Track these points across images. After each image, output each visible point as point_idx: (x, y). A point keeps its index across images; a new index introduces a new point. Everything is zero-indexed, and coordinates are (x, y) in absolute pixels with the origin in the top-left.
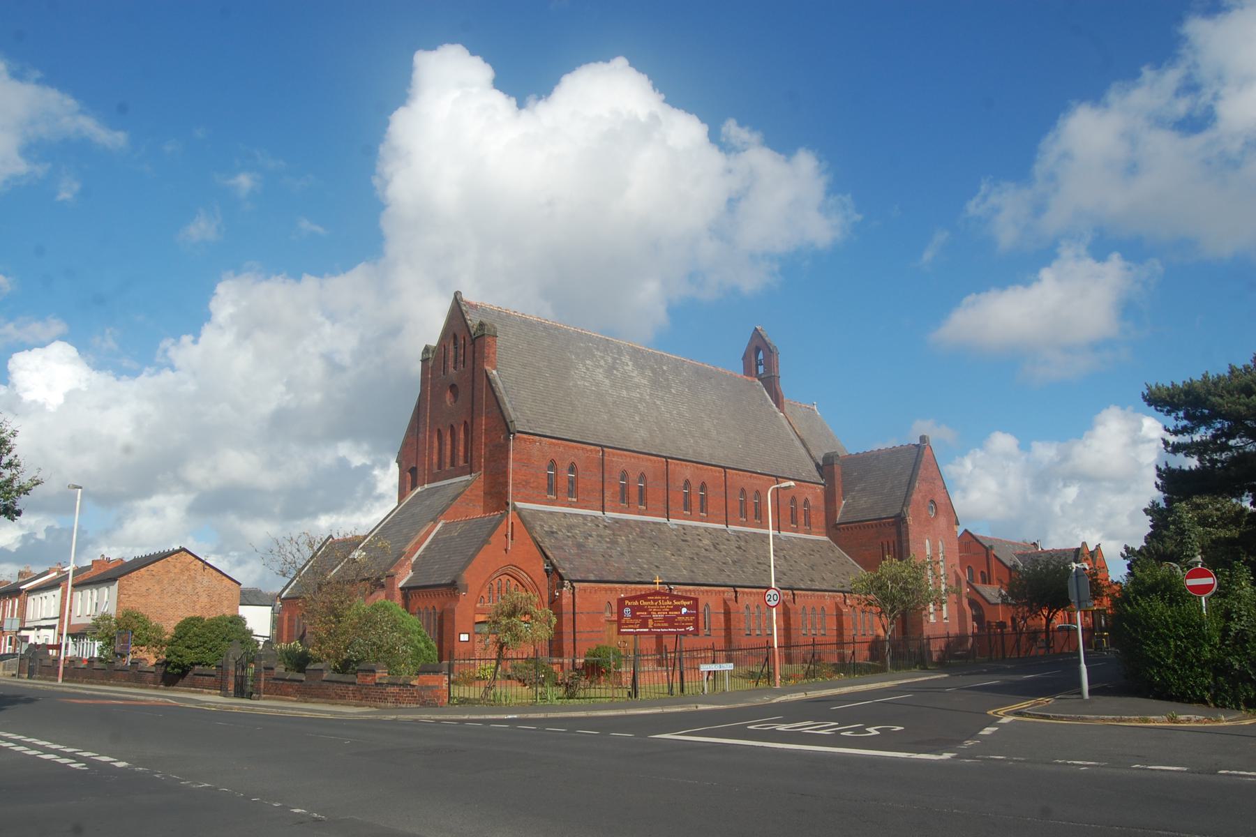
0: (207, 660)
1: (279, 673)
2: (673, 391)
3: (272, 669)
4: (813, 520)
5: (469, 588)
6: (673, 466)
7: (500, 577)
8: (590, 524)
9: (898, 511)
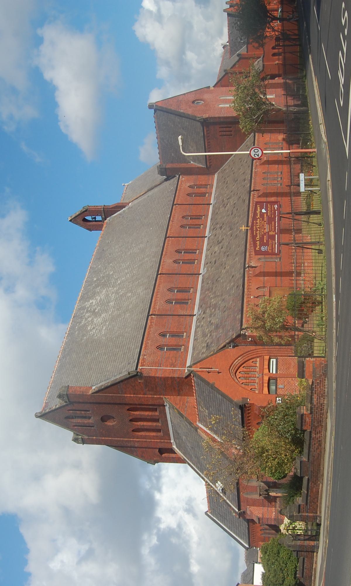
0: (293, 567)
1: (303, 501)
2: (112, 273)
3: (299, 506)
4: (203, 183)
5: (245, 397)
6: (163, 270)
7: (238, 378)
8: (202, 323)
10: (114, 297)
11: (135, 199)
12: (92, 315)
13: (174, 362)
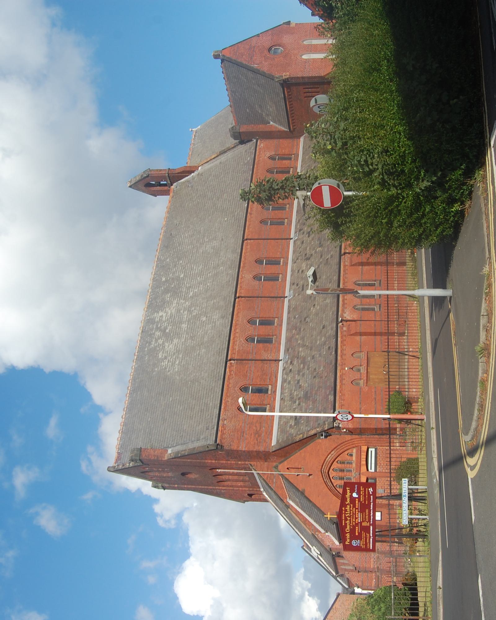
7: (331, 477)
9: (278, 85)
10: (187, 317)
11: (206, 163)
12: (163, 336)
13: (259, 429)
